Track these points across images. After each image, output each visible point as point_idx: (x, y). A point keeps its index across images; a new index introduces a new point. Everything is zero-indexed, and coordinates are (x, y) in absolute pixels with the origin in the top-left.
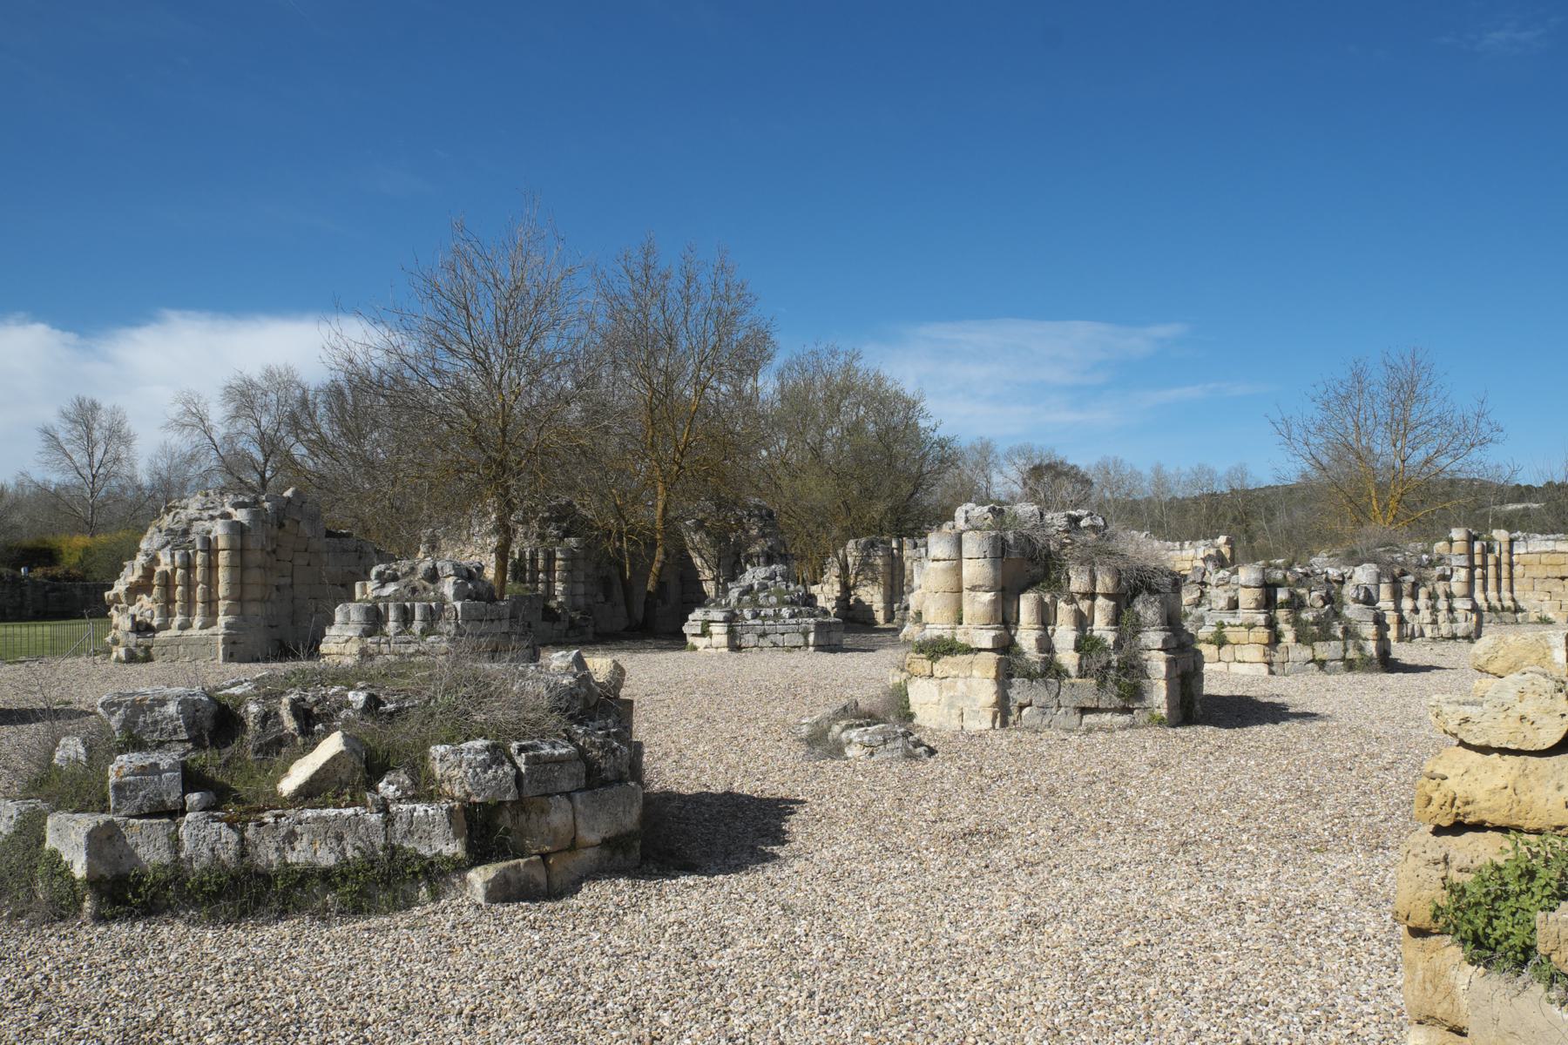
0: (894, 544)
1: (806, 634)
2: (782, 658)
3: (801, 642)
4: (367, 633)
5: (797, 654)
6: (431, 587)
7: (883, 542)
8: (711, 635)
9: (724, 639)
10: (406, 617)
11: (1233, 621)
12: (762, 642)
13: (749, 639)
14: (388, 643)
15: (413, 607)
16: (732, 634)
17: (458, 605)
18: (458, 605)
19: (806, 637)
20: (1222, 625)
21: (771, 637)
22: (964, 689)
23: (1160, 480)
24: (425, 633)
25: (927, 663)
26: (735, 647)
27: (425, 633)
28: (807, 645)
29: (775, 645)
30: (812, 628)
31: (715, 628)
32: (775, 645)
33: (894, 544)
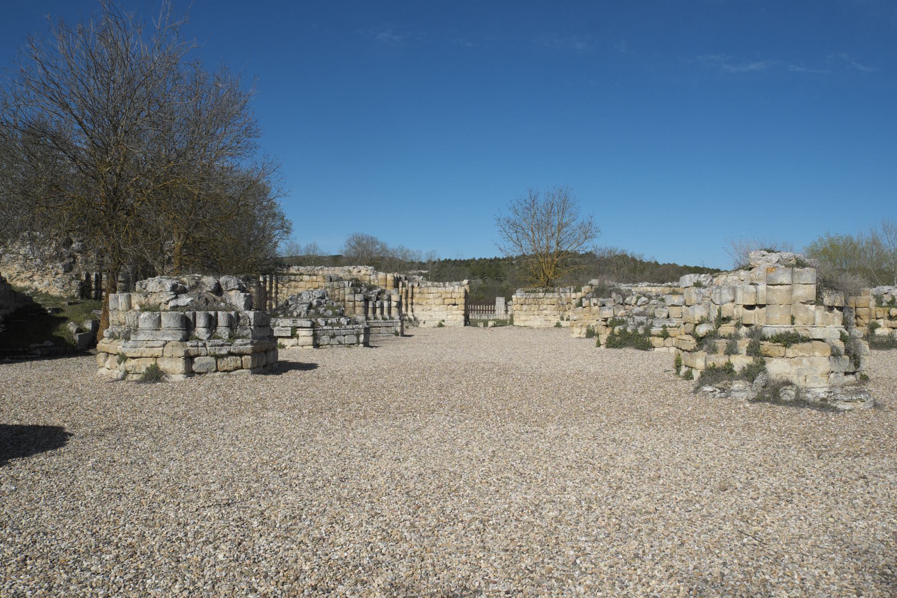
0: (261, 279)
1: (358, 335)
2: (343, 352)
3: (354, 340)
4: (186, 339)
5: (355, 349)
6: (219, 299)
7: (253, 277)
8: (298, 337)
9: (310, 340)
10: (212, 324)
11: (671, 325)
12: (333, 341)
13: (325, 339)
14: (205, 345)
15: (216, 315)
16: (315, 336)
17: (251, 314)
18: (251, 314)
19: (358, 338)
20: (664, 327)
21: (338, 338)
22: (808, 364)
23: (384, 248)
24: (232, 337)
25: (782, 349)
26: (316, 345)
27: (232, 337)
28: (358, 343)
29: (340, 343)
30: (363, 331)
31: (301, 332)
32: (340, 343)
33: (261, 279)
